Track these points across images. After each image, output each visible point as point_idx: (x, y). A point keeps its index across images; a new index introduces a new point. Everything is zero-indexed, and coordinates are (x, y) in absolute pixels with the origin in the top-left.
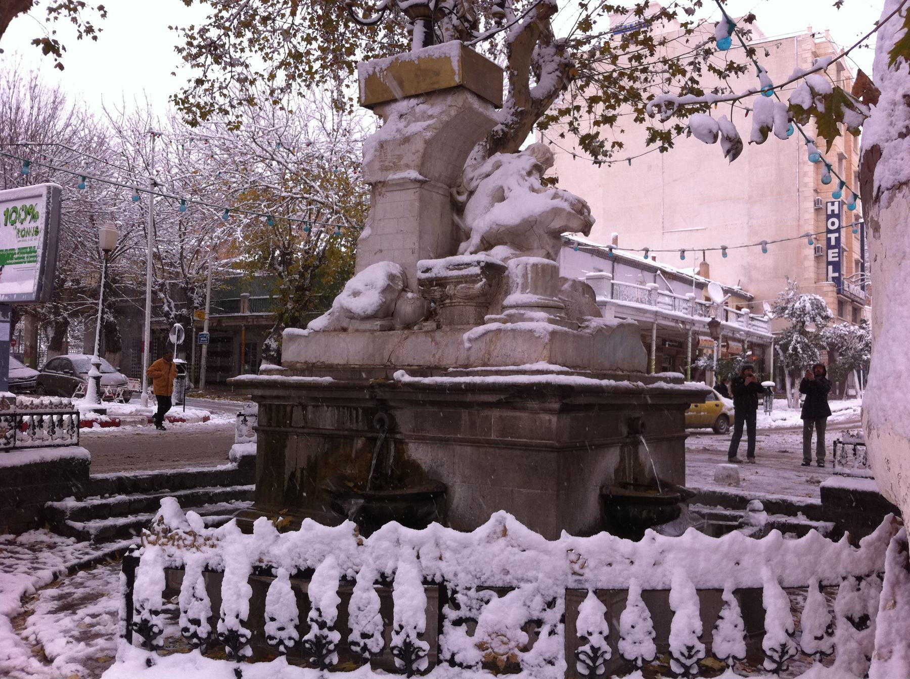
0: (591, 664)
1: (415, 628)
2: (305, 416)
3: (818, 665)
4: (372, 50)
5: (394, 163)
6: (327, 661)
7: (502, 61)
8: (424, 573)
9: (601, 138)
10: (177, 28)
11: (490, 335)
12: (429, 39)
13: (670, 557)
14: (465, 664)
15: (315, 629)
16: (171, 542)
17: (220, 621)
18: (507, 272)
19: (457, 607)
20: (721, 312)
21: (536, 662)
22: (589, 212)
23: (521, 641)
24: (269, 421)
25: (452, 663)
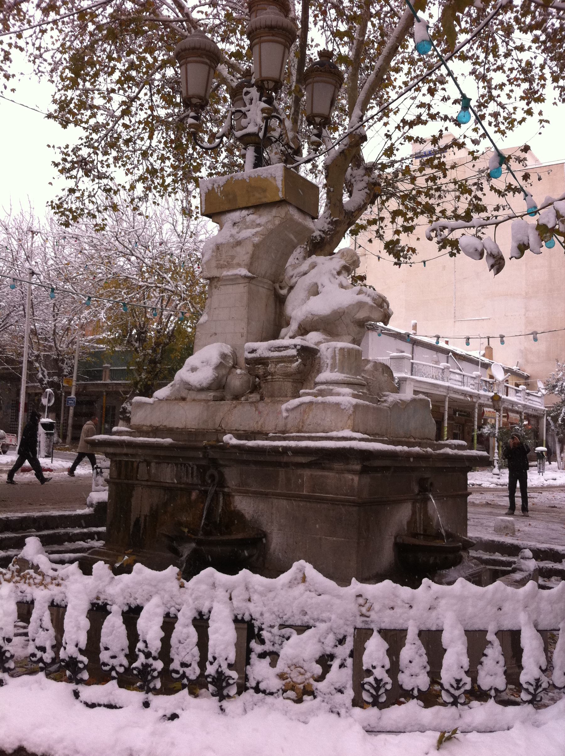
0: (374, 693)
1: (226, 659)
2: (149, 472)
4: (215, 168)
5: (228, 262)
6: (152, 686)
7: (320, 181)
8: (236, 612)
9: (402, 244)
10: (54, 147)
11: (304, 406)
12: (259, 162)
13: (443, 602)
14: (268, 691)
15: (142, 659)
16: (23, 580)
17: (62, 649)
18: (319, 355)
19: (262, 642)
20: (502, 388)
21: (328, 690)
22: (388, 306)
23: (315, 672)
24: (119, 474)
25: (257, 690)
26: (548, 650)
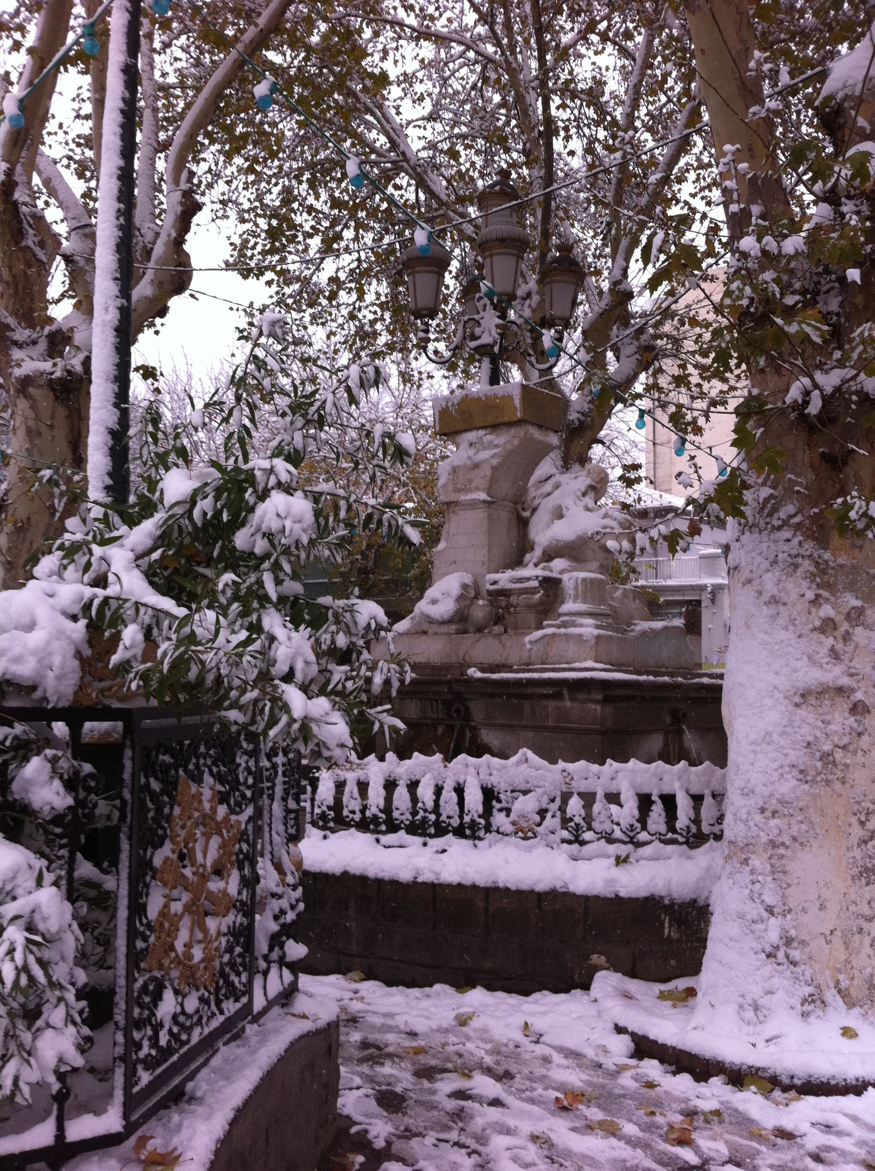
3: (712, 841)
13: (621, 774)
15: (421, 813)
25: (498, 832)
26: (697, 808)
